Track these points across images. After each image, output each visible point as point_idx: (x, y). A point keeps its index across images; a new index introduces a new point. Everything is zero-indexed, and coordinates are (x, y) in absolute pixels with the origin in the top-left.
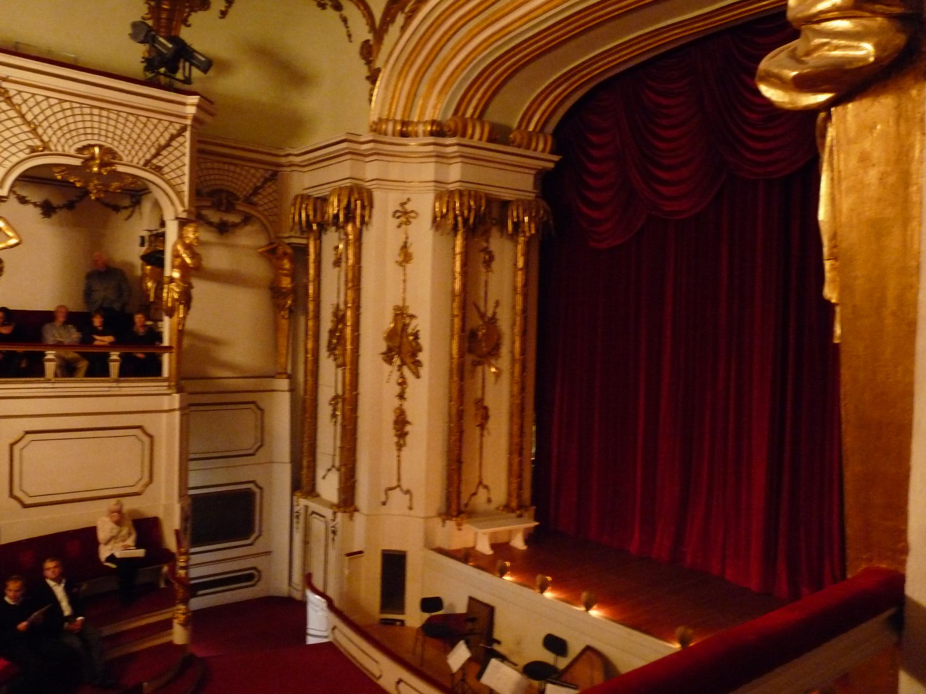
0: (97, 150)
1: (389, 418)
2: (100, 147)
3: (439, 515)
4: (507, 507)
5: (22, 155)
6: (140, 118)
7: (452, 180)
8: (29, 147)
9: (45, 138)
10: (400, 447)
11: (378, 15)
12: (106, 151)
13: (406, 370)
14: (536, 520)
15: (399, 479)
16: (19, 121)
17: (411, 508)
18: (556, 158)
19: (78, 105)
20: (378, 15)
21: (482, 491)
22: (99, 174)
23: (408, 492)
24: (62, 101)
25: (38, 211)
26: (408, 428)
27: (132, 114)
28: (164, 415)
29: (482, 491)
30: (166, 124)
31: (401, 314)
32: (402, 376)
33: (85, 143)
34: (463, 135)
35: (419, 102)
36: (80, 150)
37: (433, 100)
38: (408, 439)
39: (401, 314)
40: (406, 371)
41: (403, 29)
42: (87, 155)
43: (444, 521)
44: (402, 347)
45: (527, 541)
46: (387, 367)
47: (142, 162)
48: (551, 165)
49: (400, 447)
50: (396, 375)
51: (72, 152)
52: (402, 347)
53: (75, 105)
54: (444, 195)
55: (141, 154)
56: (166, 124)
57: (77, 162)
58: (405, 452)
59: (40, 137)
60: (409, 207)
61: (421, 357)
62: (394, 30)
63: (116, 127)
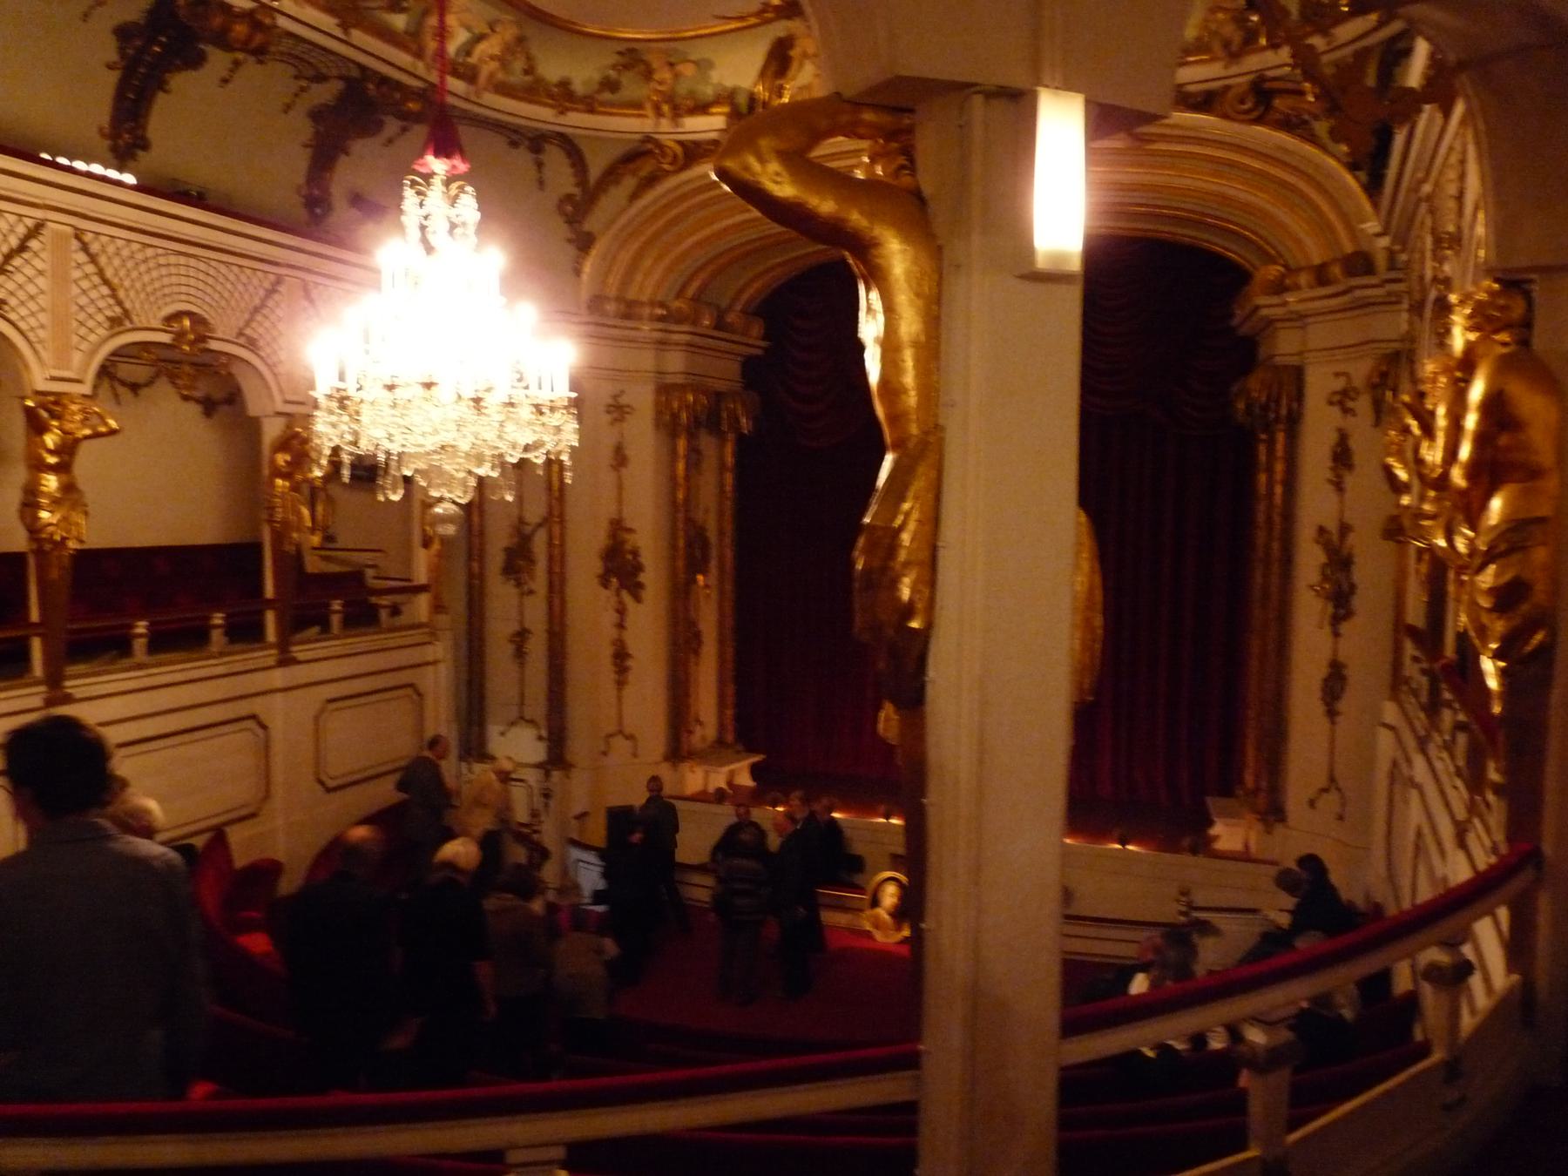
0: (187, 323)
1: (607, 652)
3: (667, 758)
4: (720, 742)
5: (102, 332)
7: (671, 370)
8: (109, 319)
9: (128, 305)
10: (621, 684)
11: (595, 172)
14: (751, 749)
16: (96, 280)
17: (635, 755)
18: (763, 344)
20: (595, 172)
21: (619, 743)
26: (629, 663)
28: (279, 696)
29: (619, 743)
31: (618, 528)
32: (621, 602)
34: (695, 322)
35: (639, 278)
36: (170, 319)
37: (657, 275)
38: (631, 677)
39: (618, 528)
40: (626, 597)
41: (634, 196)
44: (620, 567)
46: (604, 593)
48: (759, 352)
49: (621, 684)
50: (614, 600)
51: (156, 324)
52: (620, 567)
53: (160, 251)
54: (664, 390)
57: (165, 338)
58: (628, 691)
59: (120, 303)
60: (624, 400)
61: (643, 578)
62: (617, 195)
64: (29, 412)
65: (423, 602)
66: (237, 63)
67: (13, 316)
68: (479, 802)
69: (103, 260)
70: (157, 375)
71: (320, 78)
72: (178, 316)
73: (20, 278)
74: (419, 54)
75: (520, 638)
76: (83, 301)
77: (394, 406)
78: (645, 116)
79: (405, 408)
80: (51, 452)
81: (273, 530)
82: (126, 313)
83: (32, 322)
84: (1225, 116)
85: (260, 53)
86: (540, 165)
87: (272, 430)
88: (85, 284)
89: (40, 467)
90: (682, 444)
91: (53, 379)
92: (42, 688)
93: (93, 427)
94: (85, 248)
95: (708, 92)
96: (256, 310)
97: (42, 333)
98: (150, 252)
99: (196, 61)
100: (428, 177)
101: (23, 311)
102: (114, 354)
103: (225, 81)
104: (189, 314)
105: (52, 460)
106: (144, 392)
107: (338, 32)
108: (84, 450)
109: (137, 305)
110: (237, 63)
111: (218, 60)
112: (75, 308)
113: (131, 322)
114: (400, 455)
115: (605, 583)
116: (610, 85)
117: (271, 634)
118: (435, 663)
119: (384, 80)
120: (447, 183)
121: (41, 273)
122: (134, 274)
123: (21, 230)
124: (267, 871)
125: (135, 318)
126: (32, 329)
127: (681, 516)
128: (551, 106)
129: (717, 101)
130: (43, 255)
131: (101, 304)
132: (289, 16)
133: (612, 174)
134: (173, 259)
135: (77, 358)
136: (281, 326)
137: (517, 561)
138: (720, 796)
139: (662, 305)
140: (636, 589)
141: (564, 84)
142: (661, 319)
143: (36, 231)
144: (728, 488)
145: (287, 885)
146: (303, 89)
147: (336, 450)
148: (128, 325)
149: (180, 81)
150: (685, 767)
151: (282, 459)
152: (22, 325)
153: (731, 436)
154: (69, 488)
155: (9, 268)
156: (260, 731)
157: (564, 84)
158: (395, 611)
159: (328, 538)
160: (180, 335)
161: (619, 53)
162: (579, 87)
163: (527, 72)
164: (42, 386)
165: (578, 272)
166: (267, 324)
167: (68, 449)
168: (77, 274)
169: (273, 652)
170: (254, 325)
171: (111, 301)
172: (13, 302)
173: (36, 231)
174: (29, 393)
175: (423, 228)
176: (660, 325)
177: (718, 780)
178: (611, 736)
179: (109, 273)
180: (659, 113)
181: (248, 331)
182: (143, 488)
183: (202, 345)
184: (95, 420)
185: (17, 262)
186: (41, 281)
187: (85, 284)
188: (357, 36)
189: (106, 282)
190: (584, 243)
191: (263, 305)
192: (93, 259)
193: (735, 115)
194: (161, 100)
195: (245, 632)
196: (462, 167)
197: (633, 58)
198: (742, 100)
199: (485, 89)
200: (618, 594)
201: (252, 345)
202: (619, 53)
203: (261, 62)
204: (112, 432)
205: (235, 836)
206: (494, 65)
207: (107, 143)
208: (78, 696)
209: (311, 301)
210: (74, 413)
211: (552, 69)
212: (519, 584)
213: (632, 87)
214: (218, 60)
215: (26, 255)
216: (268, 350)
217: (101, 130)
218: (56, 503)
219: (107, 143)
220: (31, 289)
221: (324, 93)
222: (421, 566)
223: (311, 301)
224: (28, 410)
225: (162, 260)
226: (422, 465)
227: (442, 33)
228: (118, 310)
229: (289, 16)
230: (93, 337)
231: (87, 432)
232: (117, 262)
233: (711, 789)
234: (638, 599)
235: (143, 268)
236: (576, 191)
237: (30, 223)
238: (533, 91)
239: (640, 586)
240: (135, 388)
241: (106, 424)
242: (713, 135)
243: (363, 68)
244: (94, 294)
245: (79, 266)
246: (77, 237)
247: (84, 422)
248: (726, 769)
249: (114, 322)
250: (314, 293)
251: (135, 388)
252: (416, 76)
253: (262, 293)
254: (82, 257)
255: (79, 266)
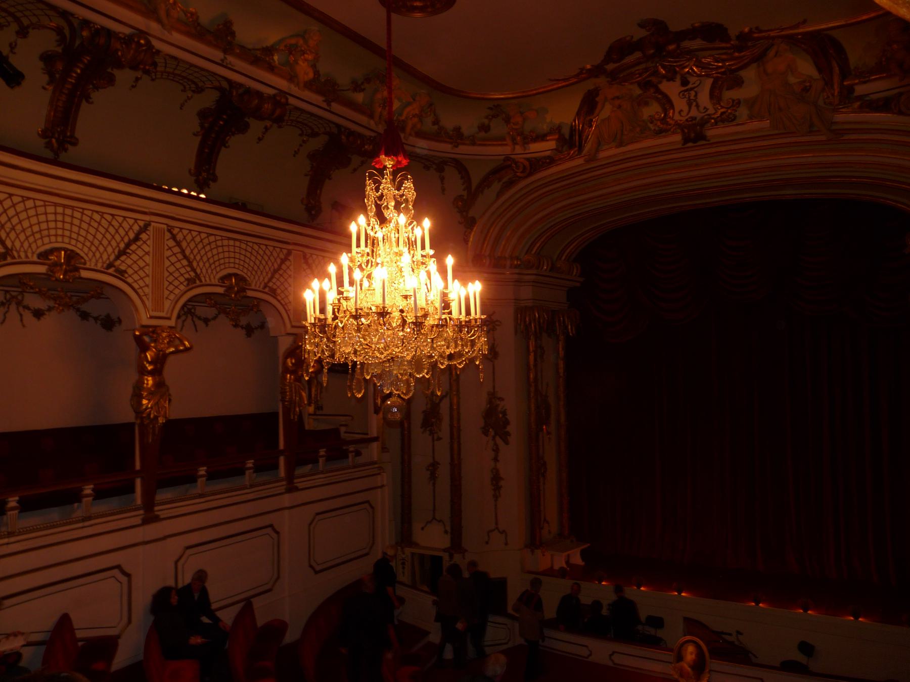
2: (66, 250)
5: (182, 287)
6: (105, 216)
8: (187, 279)
9: (198, 271)
10: (496, 497)
11: (475, 182)
12: (71, 256)
13: (498, 438)
15: (497, 523)
16: (180, 256)
17: (506, 544)
19: (42, 203)
20: (475, 182)
22: (65, 281)
23: (504, 532)
24: (25, 199)
25: (244, 332)
26: (502, 483)
27: (97, 212)
28: (286, 512)
30: (18, 199)
31: (493, 396)
32: (496, 444)
33: (48, 247)
36: (223, 279)
40: (499, 440)
41: (499, 194)
42: (227, 283)
43: (533, 552)
45: (583, 560)
47: (105, 265)
49: (496, 497)
53: (38, 203)
55: (261, 278)
56: (131, 222)
57: (220, 290)
59: (194, 270)
61: (509, 428)
63: (72, 224)
64: (138, 339)
65: (375, 446)
66: (266, 129)
67: (130, 280)
68: (306, 60)
69: (184, 244)
70: (219, 313)
71: (314, 135)
72: (229, 276)
73: (134, 257)
74: (371, 116)
75: (433, 467)
76: (172, 269)
77: (359, 330)
78: (506, 145)
79: (366, 330)
80: (150, 363)
81: (284, 407)
82: (198, 276)
83: (141, 283)
84: (900, 113)
85: (279, 121)
86: (442, 179)
87: (285, 344)
88: (173, 259)
89: (143, 372)
90: (532, 343)
91: (151, 317)
92: (142, 512)
93: (176, 347)
94: (174, 237)
95: (545, 128)
96: (276, 271)
97: (146, 290)
98: (212, 239)
99: (244, 128)
100: (381, 171)
101: (136, 277)
102: (190, 300)
103: (260, 139)
104: (236, 275)
105: (150, 368)
106: (211, 323)
107: (324, 105)
108: (171, 360)
109: (204, 271)
110: (266, 129)
111: (256, 127)
112: (166, 274)
113: (201, 281)
114: (362, 364)
115: (485, 432)
116: (484, 128)
117: (282, 472)
118: (382, 486)
119: (351, 133)
120: (394, 174)
121: (147, 253)
122: (203, 252)
123: (136, 228)
124: (278, 628)
125: (203, 279)
126: (141, 288)
127: (532, 389)
128: (451, 143)
129: (550, 133)
130: (148, 242)
131: (183, 271)
132: (297, 98)
133: (486, 182)
134: (226, 242)
135: (167, 304)
136: (290, 280)
137: (431, 418)
138: (562, 573)
139: (517, 259)
140: (505, 436)
141: (458, 130)
142: (516, 267)
143: (144, 229)
144: (561, 371)
145: (290, 637)
146: (304, 142)
147: (319, 361)
148: (198, 282)
149: (235, 141)
150: (538, 552)
151: (290, 362)
152: (136, 286)
153: (562, 337)
154: (160, 385)
155: (128, 251)
156: (274, 535)
157: (458, 130)
158: (358, 453)
159: (319, 408)
160: (230, 288)
161: (490, 108)
162: (466, 131)
163: (434, 123)
164: (145, 321)
165: (466, 241)
166: (282, 280)
167: (160, 360)
168: (169, 253)
169: (284, 483)
170: (274, 280)
171: (189, 269)
172: (130, 271)
173: (144, 229)
174: (137, 326)
175: (378, 207)
176: (517, 271)
177: (559, 562)
178: (492, 531)
179: (188, 252)
180: (514, 143)
181: (271, 284)
182: (208, 381)
183: (242, 294)
184: (177, 342)
185: (133, 247)
186: (147, 258)
187: (173, 259)
188: (335, 107)
189: (185, 257)
190: (470, 223)
191: (280, 268)
192: (178, 244)
193: (561, 140)
194: (223, 151)
195: (267, 466)
196: (405, 162)
197: (497, 110)
198: (566, 132)
199: (410, 135)
200: (494, 438)
201: (273, 293)
202: (490, 108)
203: (280, 127)
204: (187, 349)
205: (257, 603)
206: (416, 120)
207: (194, 178)
208: (162, 517)
209: (307, 262)
210: (164, 338)
211: (449, 122)
212: (432, 433)
213: (498, 128)
214: (256, 127)
215: (139, 243)
216: (283, 295)
217: (190, 171)
218: (151, 394)
219: (194, 178)
220: (141, 263)
221: (317, 144)
222: (374, 425)
223: (307, 262)
224: (136, 337)
225: (219, 243)
226: (377, 371)
227: (388, 102)
228: (192, 274)
229: (297, 98)
230: (177, 291)
231: (172, 349)
232: (192, 245)
233: (556, 567)
234: (507, 443)
235: (208, 248)
236: (465, 193)
237: (142, 224)
238: (438, 136)
239: (508, 434)
240: (206, 321)
241: (184, 345)
242: (548, 153)
243: (338, 126)
244: (178, 265)
245: (170, 248)
246: (169, 231)
247: (170, 344)
248: (566, 553)
249: (190, 281)
250: (310, 261)
251: (206, 321)
252: (372, 130)
253: (279, 261)
254: (171, 243)
255: (170, 248)
